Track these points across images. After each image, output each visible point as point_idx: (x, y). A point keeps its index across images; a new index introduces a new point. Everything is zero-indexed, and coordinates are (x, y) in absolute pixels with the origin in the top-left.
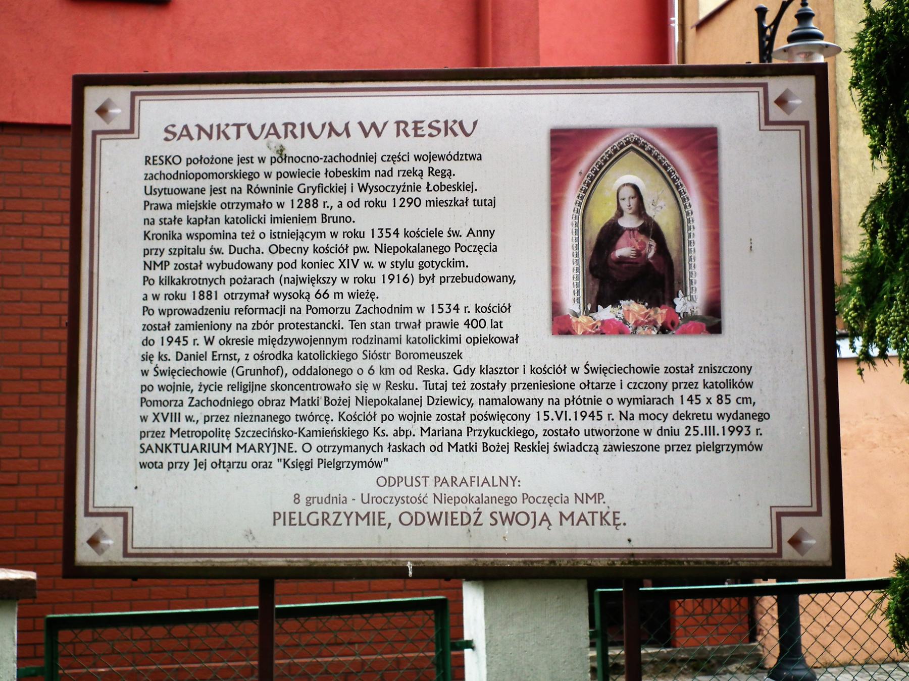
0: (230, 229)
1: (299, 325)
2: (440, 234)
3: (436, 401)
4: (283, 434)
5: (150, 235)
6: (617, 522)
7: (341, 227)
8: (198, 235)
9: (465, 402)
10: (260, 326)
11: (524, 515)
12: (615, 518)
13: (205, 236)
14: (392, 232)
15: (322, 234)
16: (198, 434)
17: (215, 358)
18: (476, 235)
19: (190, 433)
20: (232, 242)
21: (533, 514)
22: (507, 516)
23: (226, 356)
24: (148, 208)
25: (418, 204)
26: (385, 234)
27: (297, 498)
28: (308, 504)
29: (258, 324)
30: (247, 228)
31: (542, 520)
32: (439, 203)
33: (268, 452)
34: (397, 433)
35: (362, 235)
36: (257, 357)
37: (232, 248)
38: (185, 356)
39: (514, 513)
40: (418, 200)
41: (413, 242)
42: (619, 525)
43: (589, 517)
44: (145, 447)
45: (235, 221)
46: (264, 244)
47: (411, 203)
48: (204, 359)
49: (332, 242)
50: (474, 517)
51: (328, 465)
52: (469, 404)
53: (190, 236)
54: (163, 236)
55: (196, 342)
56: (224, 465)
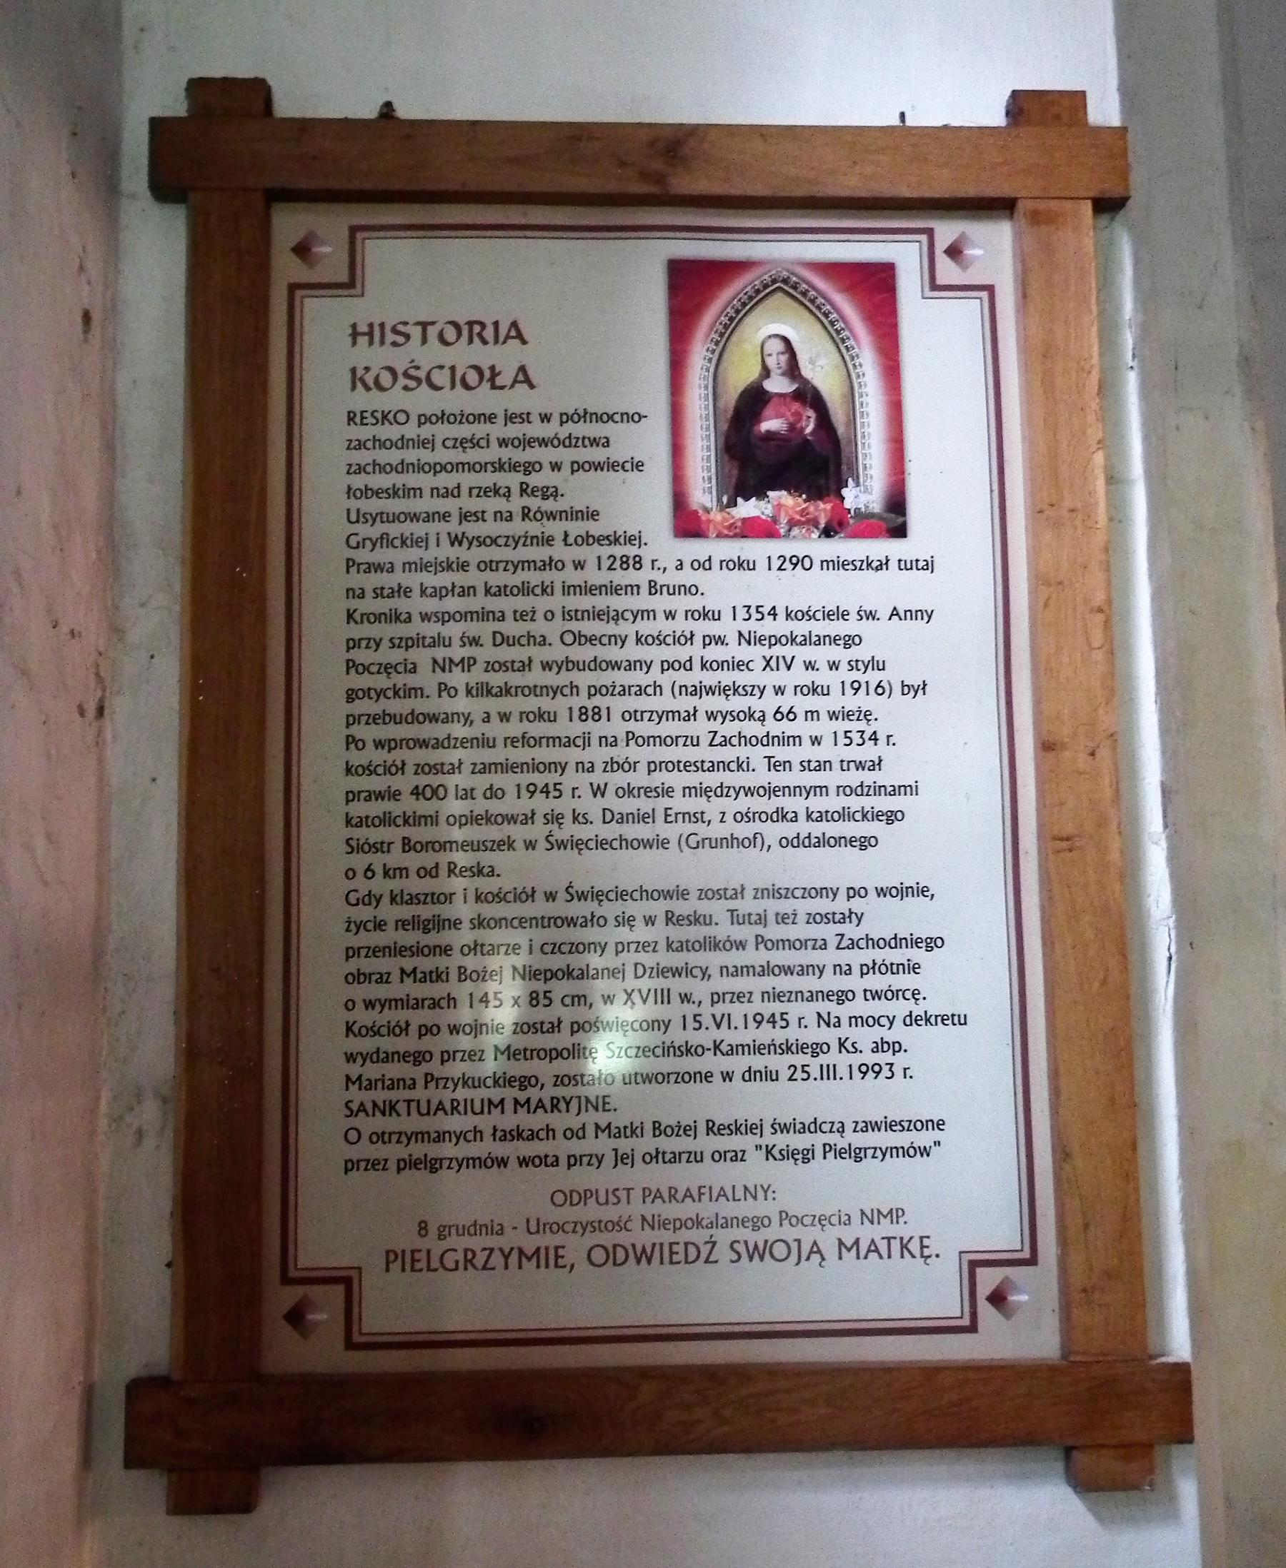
0: (494, 604)
1: (682, 765)
2: (844, 615)
3: (648, 971)
4: (688, 1051)
5: (357, 616)
6: (926, 1252)
7: (681, 603)
8: (440, 615)
9: (697, 972)
10: (615, 766)
11: (783, 1244)
12: (922, 1247)
13: (452, 617)
14: (765, 610)
15: (649, 614)
16: (542, 1054)
17: (669, 819)
18: (903, 617)
19: (528, 1053)
20: (498, 626)
21: (796, 1243)
22: (756, 1247)
23: (687, 816)
24: (353, 570)
25: (807, 565)
26: (756, 616)
27: (423, 1227)
28: (441, 1237)
29: (612, 763)
30: (523, 603)
31: (811, 1252)
32: (841, 565)
33: (568, 1111)
34: (877, 1047)
35: (717, 617)
36: (739, 817)
37: (498, 635)
38: (617, 817)
39: (766, 1242)
40: (807, 560)
41: (801, 628)
42: (930, 1257)
43: (883, 1246)
44: (355, 1107)
45: (502, 591)
46: (553, 630)
47: (796, 565)
48: (650, 820)
49: (666, 627)
50: (705, 1250)
51: (840, 1154)
52: (704, 974)
53: (425, 617)
54: (378, 617)
55: (577, 793)
56: (663, 1158)
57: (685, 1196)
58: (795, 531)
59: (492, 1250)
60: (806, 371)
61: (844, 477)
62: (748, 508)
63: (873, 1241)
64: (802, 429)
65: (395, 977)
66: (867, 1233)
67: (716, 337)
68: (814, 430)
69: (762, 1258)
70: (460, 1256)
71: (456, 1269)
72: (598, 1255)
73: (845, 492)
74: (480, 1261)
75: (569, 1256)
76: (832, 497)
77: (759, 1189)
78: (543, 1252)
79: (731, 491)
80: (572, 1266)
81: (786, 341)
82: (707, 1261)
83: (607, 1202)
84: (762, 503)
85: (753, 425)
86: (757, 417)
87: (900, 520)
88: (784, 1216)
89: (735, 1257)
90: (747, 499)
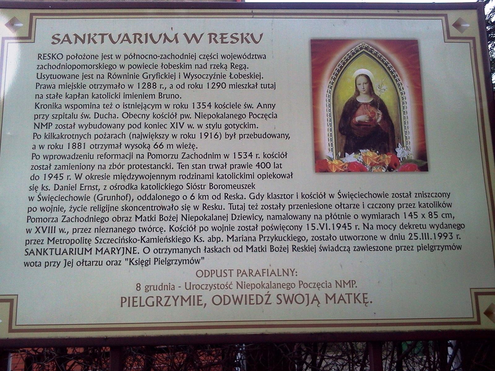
12: (364, 298)
22: (289, 297)
27: (138, 287)
28: (147, 291)
31: (313, 300)
39: (293, 295)
42: (368, 302)
43: (346, 297)
50: (265, 298)
57: (256, 274)
58: (374, 169)
59: (169, 297)
60: (377, 93)
61: (396, 142)
62: (351, 158)
63: (341, 295)
64: (376, 120)
65: (133, 219)
66: (339, 291)
67: (334, 76)
68: (381, 120)
69: (291, 302)
70: (155, 300)
71: (153, 305)
72: (217, 300)
73: (397, 150)
74: (163, 302)
75: (204, 300)
76: (391, 152)
77: (289, 270)
78: (192, 298)
79: (342, 150)
80: (205, 304)
81: (367, 77)
82: (266, 303)
83: (221, 276)
84: (357, 156)
85: (351, 119)
86: (354, 115)
87: (425, 163)
88: (301, 283)
89: (279, 302)
90: (350, 153)
